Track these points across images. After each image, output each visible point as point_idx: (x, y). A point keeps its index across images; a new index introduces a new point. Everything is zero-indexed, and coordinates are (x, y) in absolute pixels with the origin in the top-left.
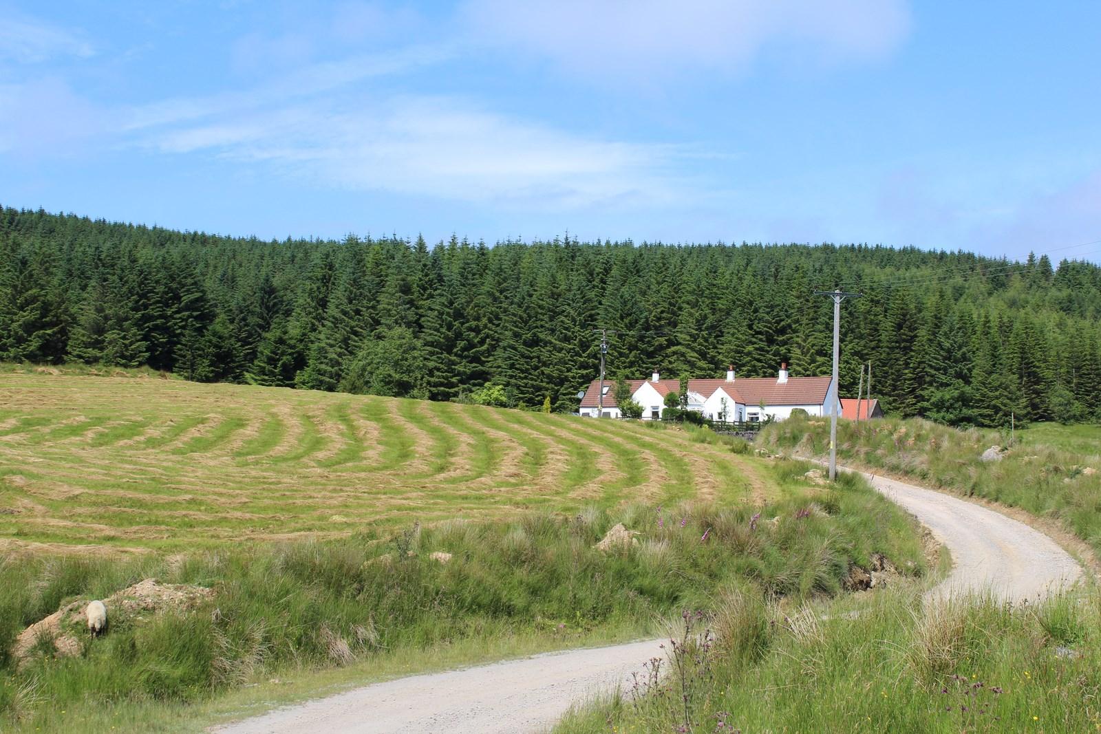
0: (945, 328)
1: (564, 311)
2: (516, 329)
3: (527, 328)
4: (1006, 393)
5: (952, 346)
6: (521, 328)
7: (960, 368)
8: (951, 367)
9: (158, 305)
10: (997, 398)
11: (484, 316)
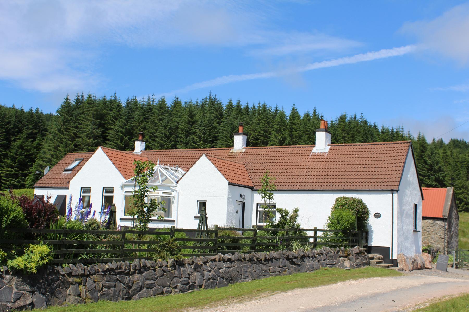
0: (428, 152)
1: (195, 133)
2: (161, 142)
3: (169, 141)
4: (466, 191)
5: (433, 163)
6: (164, 141)
7: (438, 176)
8: (432, 175)
9: (4, 134)
10: (461, 194)
11: (147, 135)
